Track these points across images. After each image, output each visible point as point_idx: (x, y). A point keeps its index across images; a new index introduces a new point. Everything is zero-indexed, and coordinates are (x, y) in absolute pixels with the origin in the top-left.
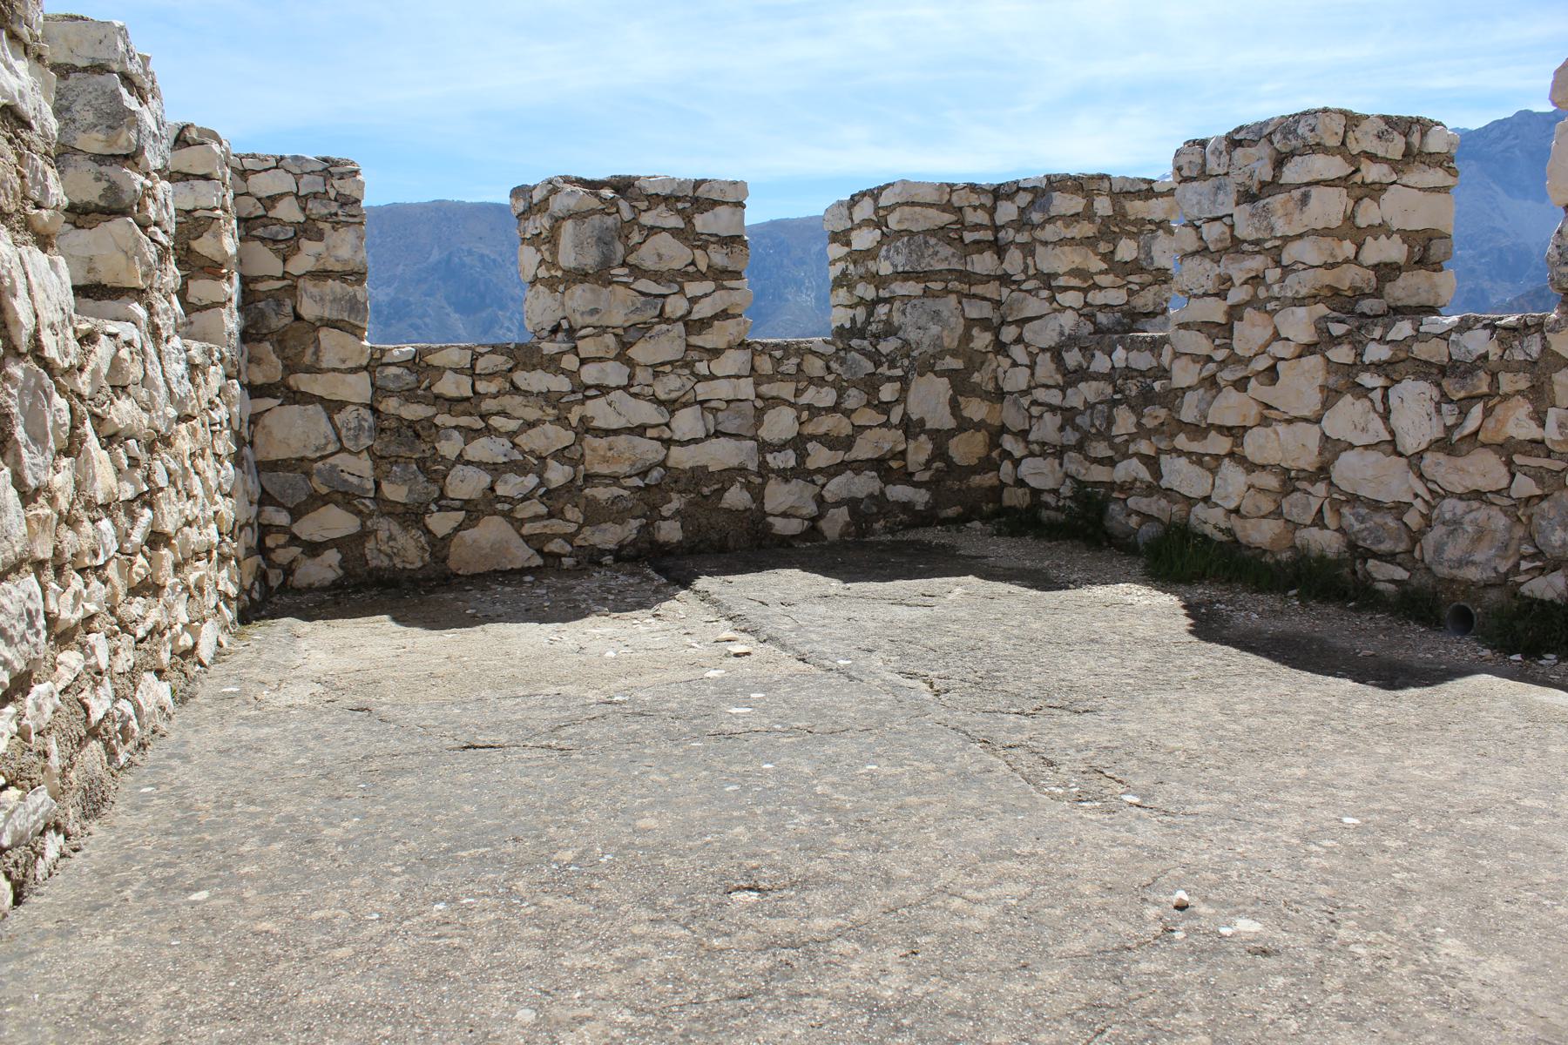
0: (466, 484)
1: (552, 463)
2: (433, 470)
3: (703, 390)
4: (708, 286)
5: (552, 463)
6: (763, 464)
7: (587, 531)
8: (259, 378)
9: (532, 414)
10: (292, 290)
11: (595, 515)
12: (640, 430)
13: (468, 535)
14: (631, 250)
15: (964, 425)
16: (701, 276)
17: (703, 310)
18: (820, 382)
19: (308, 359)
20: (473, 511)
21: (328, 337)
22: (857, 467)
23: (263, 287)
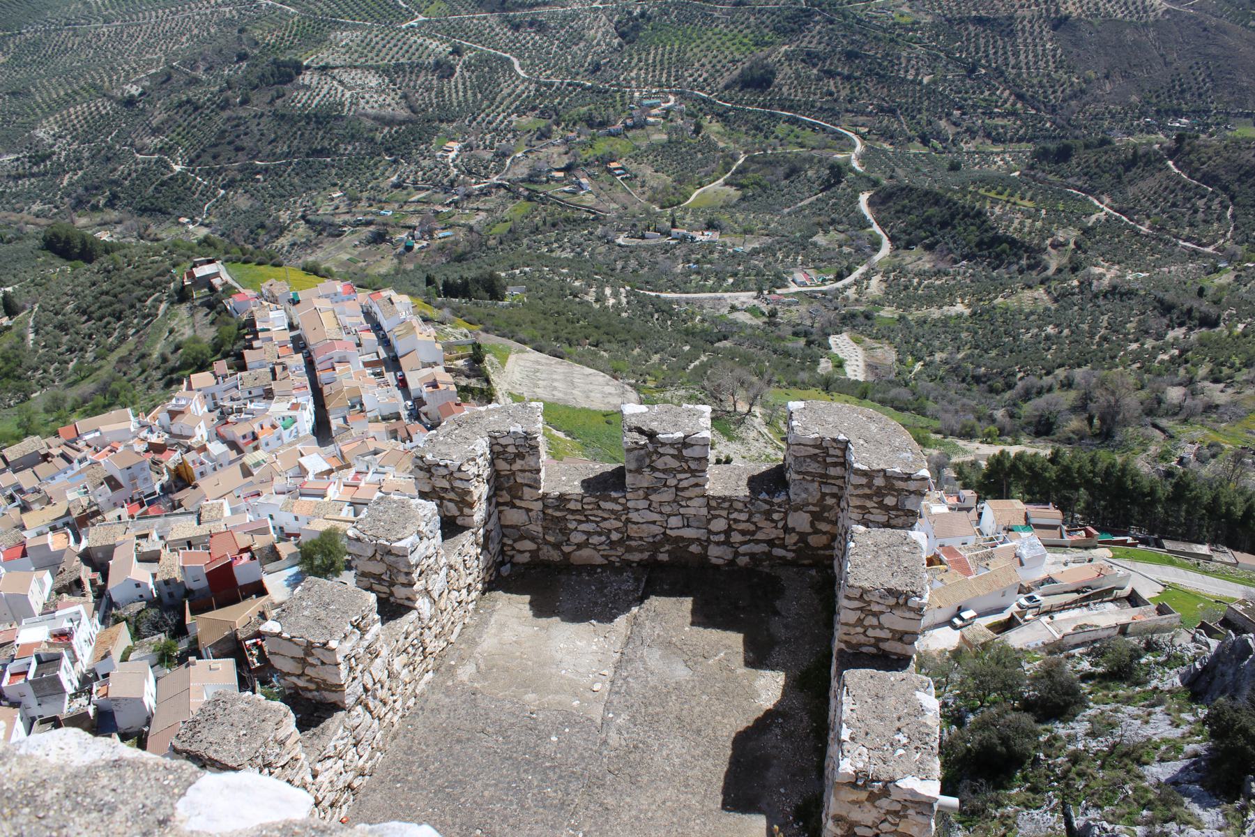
0: (577, 538)
2: (565, 532)
3: (682, 511)
4: (688, 475)
9: (606, 516)
10: (514, 474)
11: (629, 549)
12: (654, 523)
15: (816, 531)
16: (684, 471)
17: (684, 484)
18: (741, 511)
20: (579, 546)
21: (526, 489)
22: (758, 542)
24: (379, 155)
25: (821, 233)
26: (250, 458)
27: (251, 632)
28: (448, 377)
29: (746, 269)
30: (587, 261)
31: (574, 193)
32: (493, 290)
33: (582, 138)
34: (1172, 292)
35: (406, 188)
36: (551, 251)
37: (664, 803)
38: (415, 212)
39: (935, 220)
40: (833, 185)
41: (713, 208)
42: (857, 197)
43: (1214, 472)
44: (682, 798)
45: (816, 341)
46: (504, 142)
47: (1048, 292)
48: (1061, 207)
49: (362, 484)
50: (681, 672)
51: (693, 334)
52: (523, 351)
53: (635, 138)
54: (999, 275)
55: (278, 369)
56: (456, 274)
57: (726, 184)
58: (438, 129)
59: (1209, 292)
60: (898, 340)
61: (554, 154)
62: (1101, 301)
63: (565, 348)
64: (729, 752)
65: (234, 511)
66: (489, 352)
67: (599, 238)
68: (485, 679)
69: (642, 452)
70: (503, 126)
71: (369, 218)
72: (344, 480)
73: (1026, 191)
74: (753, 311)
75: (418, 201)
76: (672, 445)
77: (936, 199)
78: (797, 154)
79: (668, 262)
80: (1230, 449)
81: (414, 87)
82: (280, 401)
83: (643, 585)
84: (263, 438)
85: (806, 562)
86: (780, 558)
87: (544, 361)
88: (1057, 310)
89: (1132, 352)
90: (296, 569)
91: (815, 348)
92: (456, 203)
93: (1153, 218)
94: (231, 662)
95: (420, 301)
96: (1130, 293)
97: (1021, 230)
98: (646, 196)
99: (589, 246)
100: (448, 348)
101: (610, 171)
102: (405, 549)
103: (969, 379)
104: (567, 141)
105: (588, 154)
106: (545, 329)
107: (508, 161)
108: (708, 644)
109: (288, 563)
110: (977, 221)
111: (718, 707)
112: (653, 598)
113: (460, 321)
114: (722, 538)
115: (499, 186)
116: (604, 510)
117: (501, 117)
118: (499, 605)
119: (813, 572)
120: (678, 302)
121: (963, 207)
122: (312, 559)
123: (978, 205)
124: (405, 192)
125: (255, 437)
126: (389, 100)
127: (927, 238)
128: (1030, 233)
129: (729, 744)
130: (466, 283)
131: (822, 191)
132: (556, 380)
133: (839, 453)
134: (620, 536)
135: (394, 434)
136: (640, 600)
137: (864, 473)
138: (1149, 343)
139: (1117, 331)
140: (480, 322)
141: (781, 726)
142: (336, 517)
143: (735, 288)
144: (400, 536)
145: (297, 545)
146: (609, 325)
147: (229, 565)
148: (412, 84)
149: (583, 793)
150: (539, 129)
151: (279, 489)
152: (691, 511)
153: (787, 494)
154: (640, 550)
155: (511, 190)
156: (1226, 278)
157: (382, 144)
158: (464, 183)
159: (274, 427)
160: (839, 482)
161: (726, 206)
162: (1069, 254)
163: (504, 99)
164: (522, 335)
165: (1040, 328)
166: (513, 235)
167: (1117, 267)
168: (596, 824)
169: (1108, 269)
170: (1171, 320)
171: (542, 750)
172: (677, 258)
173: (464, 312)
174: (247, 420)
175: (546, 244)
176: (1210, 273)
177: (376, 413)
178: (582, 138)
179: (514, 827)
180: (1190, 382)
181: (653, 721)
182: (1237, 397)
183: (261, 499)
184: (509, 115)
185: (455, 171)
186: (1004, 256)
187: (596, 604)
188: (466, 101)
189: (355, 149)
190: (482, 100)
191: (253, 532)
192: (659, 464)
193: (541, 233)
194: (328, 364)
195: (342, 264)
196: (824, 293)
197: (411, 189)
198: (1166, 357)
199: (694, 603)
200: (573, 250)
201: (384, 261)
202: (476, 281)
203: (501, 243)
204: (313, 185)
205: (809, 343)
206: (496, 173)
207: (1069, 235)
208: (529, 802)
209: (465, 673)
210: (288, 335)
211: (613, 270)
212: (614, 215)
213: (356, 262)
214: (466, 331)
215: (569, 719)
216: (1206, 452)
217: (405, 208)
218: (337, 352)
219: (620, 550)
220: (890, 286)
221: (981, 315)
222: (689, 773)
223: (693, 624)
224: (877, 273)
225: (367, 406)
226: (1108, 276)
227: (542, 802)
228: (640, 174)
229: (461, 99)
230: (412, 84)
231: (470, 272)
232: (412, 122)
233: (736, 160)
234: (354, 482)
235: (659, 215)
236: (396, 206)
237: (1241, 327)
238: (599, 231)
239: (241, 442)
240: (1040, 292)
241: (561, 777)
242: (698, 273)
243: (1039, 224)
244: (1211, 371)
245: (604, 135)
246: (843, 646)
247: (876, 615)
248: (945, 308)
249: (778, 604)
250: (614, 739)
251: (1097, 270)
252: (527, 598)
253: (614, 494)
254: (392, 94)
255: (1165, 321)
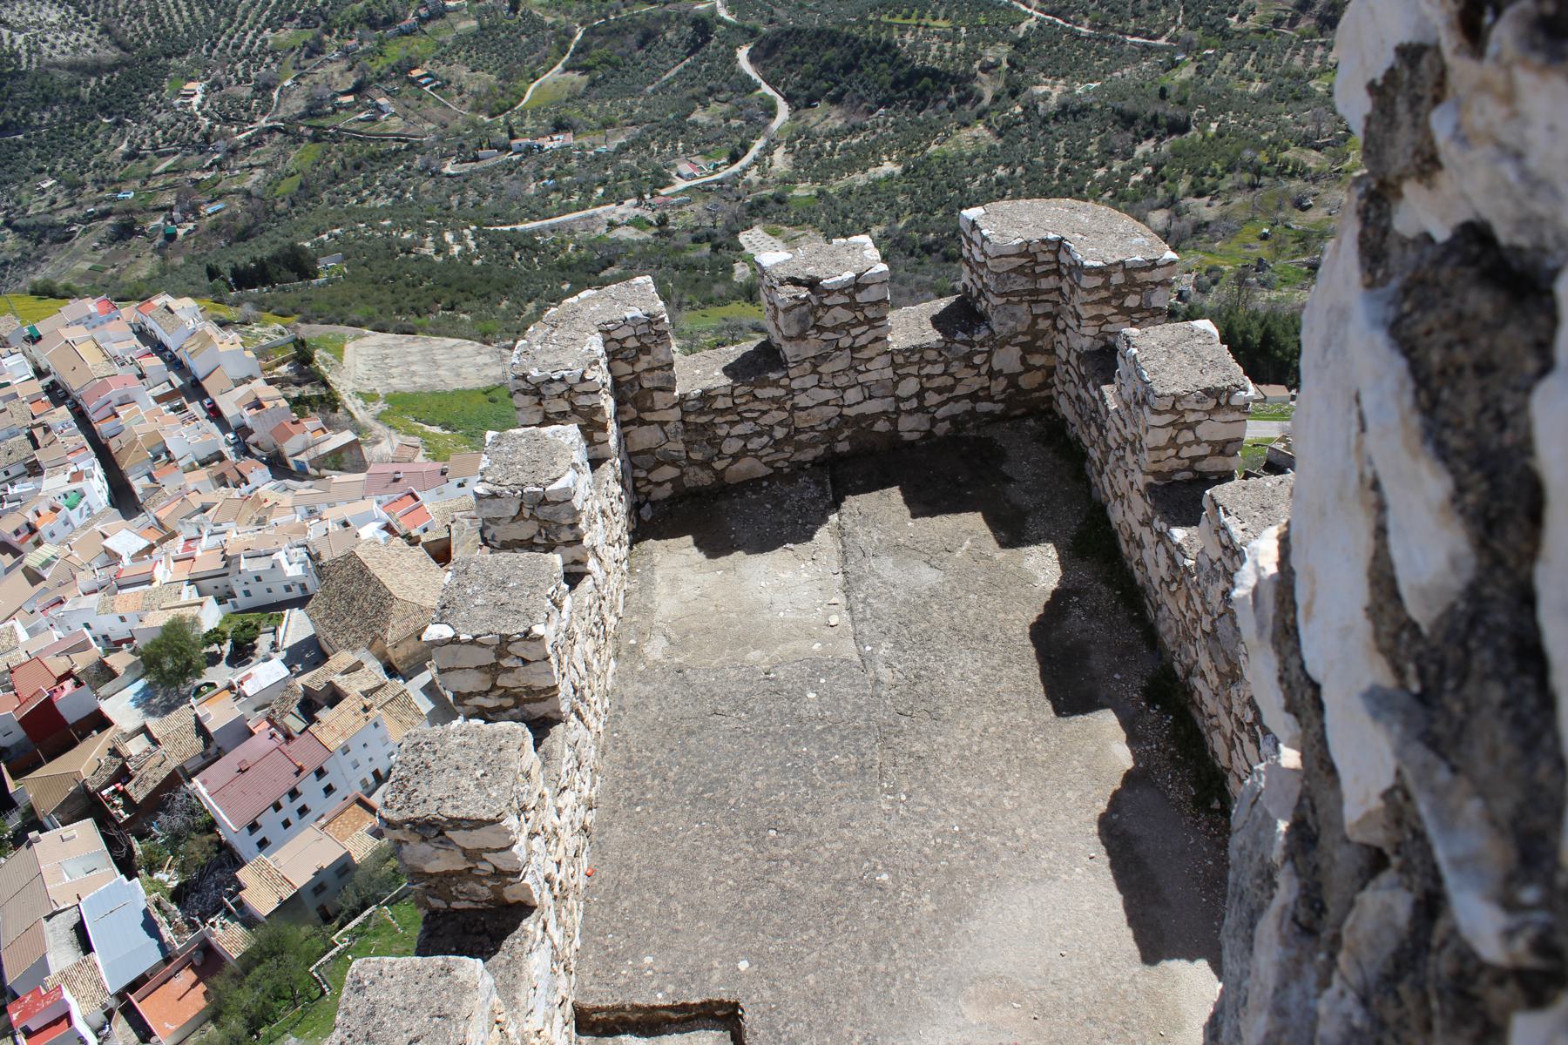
0: (730, 447)
1: (777, 428)
2: (715, 442)
3: (861, 378)
5: (777, 428)
6: (897, 408)
7: (797, 454)
8: (625, 418)
9: (765, 407)
11: (800, 447)
12: (826, 403)
13: (733, 468)
14: (819, 319)
15: (1029, 369)
16: (860, 324)
17: (862, 341)
18: (935, 362)
19: (649, 403)
20: (735, 457)
21: (657, 395)
22: (957, 399)
23: (623, 379)
24: (92, 118)
25: (699, 109)
26: (33, 559)
27: (105, 778)
28: (274, 391)
29: (616, 172)
30: (411, 205)
31: (373, 120)
32: (299, 265)
33: (367, 45)
34: (1131, 100)
35: (144, 157)
36: (362, 201)
37: (985, 730)
38: (166, 187)
39: (835, 65)
40: (702, 45)
41: (557, 103)
42: (735, 54)
43: (1218, 301)
44: (1005, 718)
45: (724, 244)
46: (263, 70)
47: (990, 128)
48: (982, 20)
49: (198, 554)
50: (928, 577)
51: (570, 267)
52: (361, 336)
53: (435, 33)
54: (927, 117)
55: (38, 433)
56: (246, 255)
57: (567, 69)
58: (166, 68)
59: (1172, 92)
60: (822, 221)
61: (334, 74)
62: (1052, 126)
63: (414, 320)
64: (1033, 651)
65: (32, 632)
66: (318, 347)
67: (421, 172)
68: (685, 650)
69: (805, 309)
70: (255, 48)
71: (103, 207)
72: (173, 554)
73: (938, 8)
74: (638, 223)
75: (166, 172)
76: (841, 291)
77: (832, 39)
78: (648, 14)
79: (516, 184)
80: (1230, 271)
81: (116, 14)
82: (53, 474)
83: (829, 487)
84: (44, 528)
85: (1018, 412)
86: (987, 414)
87: (390, 342)
88: (1003, 147)
89: (1100, 179)
90: (141, 683)
91: (724, 253)
92: (218, 163)
93: (1092, 15)
94: (89, 823)
95: (207, 302)
96: (1084, 110)
97: (941, 56)
98: (468, 104)
99: (409, 184)
100: (262, 353)
101: (413, 82)
102: (567, 489)
103: (918, 250)
104: (346, 53)
105: (379, 65)
106: (381, 302)
107: (275, 95)
108: (945, 534)
109: (129, 678)
110: (888, 57)
111: (994, 603)
112: (850, 499)
113: (267, 316)
114: (914, 403)
115: (271, 131)
116: (761, 400)
117: (249, 37)
118: (657, 558)
119: (1031, 423)
120: (540, 232)
121: (867, 42)
122: (159, 664)
123: (883, 36)
124: (144, 163)
125: (32, 529)
126: (84, 39)
127: (830, 89)
128: (953, 59)
129: (1028, 642)
130: (262, 265)
131: (688, 55)
132: (413, 363)
133: (1050, 257)
134: (785, 430)
135: (222, 480)
136: (836, 505)
137: (1099, 271)
138: (1117, 166)
139: (1078, 158)
140: (295, 311)
141: (1079, 605)
142: (175, 603)
143: (606, 199)
144: (553, 475)
145: (133, 652)
146: (462, 279)
147: (49, 701)
148: (111, 10)
149: (881, 749)
150: (305, 43)
151: (87, 589)
152: (873, 376)
153: (989, 328)
154: (812, 444)
155: (288, 130)
156: (1186, 73)
157: (92, 102)
158: (223, 135)
159: (55, 510)
160: (1054, 296)
161: (574, 98)
162: (1003, 76)
163: (247, 11)
164: (355, 316)
165: (989, 172)
166: (307, 191)
167: (1062, 81)
168: (916, 779)
169: (1053, 86)
170: (1136, 133)
171: (804, 713)
172: (526, 176)
173: (269, 303)
174: (13, 509)
175: (354, 194)
176: (1167, 70)
177: (191, 459)
178: (367, 45)
179: (815, 813)
180: (1171, 202)
181: (924, 640)
182: (1226, 209)
183: (66, 607)
184: (260, 32)
185: (207, 121)
186: (928, 93)
187: (781, 524)
188: (195, 22)
189: (54, 115)
190: (217, 19)
191: (67, 652)
192: (827, 320)
193: (343, 181)
194: (106, 411)
195: (84, 276)
196: (720, 182)
197: (152, 156)
198: (1139, 178)
199: (904, 492)
200: (390, 195)
201: (141, 261)
202: (275, 259)
203: (293, 205)
204: (8, 177)
205: (715, 248)
206: (263, 114)
207: (999, 53)
208: (819, 779)
209: (655, 649)
210: (38, 386)
211: (448, 209)
212: (432, 138)
213: (102, 270)
214: (279, 327)
215: (817, 668)
216: (1205, 279)
217: (151, 184)
218: (114, 393)
219: (789, 449)
220: (798, 157)
221: (915, 170)
222: (998, 688)
223: (914, 516)
224: (779, 144)
225: (176, 452)
226: (1055, 94)
227: (835, 772)
228: (454, 78)
229: (188, 21)
230: (111, 10)
231: (262, 248)
232: (126, 65)
233: (572, 36)
234: (187, 554)
235: (490, 127)
236: (137, 183)
237: (1214, 126)
238: (418, 162)
239: (15, 540)
240: (979, 129)
241: (843, 738)
242: (557, 190)
243: (961, 46)
244: (1192, 184)
245: (393, 36)
246: (1151, 479)
247: (1191, 427)
248: (871, 170)
249: (1004, 468)
250: (886, 675)
251: (1041, 90)
252: (689, 539)
253: (773, 376)
254: (87, 29)
255: (1130, 135)
